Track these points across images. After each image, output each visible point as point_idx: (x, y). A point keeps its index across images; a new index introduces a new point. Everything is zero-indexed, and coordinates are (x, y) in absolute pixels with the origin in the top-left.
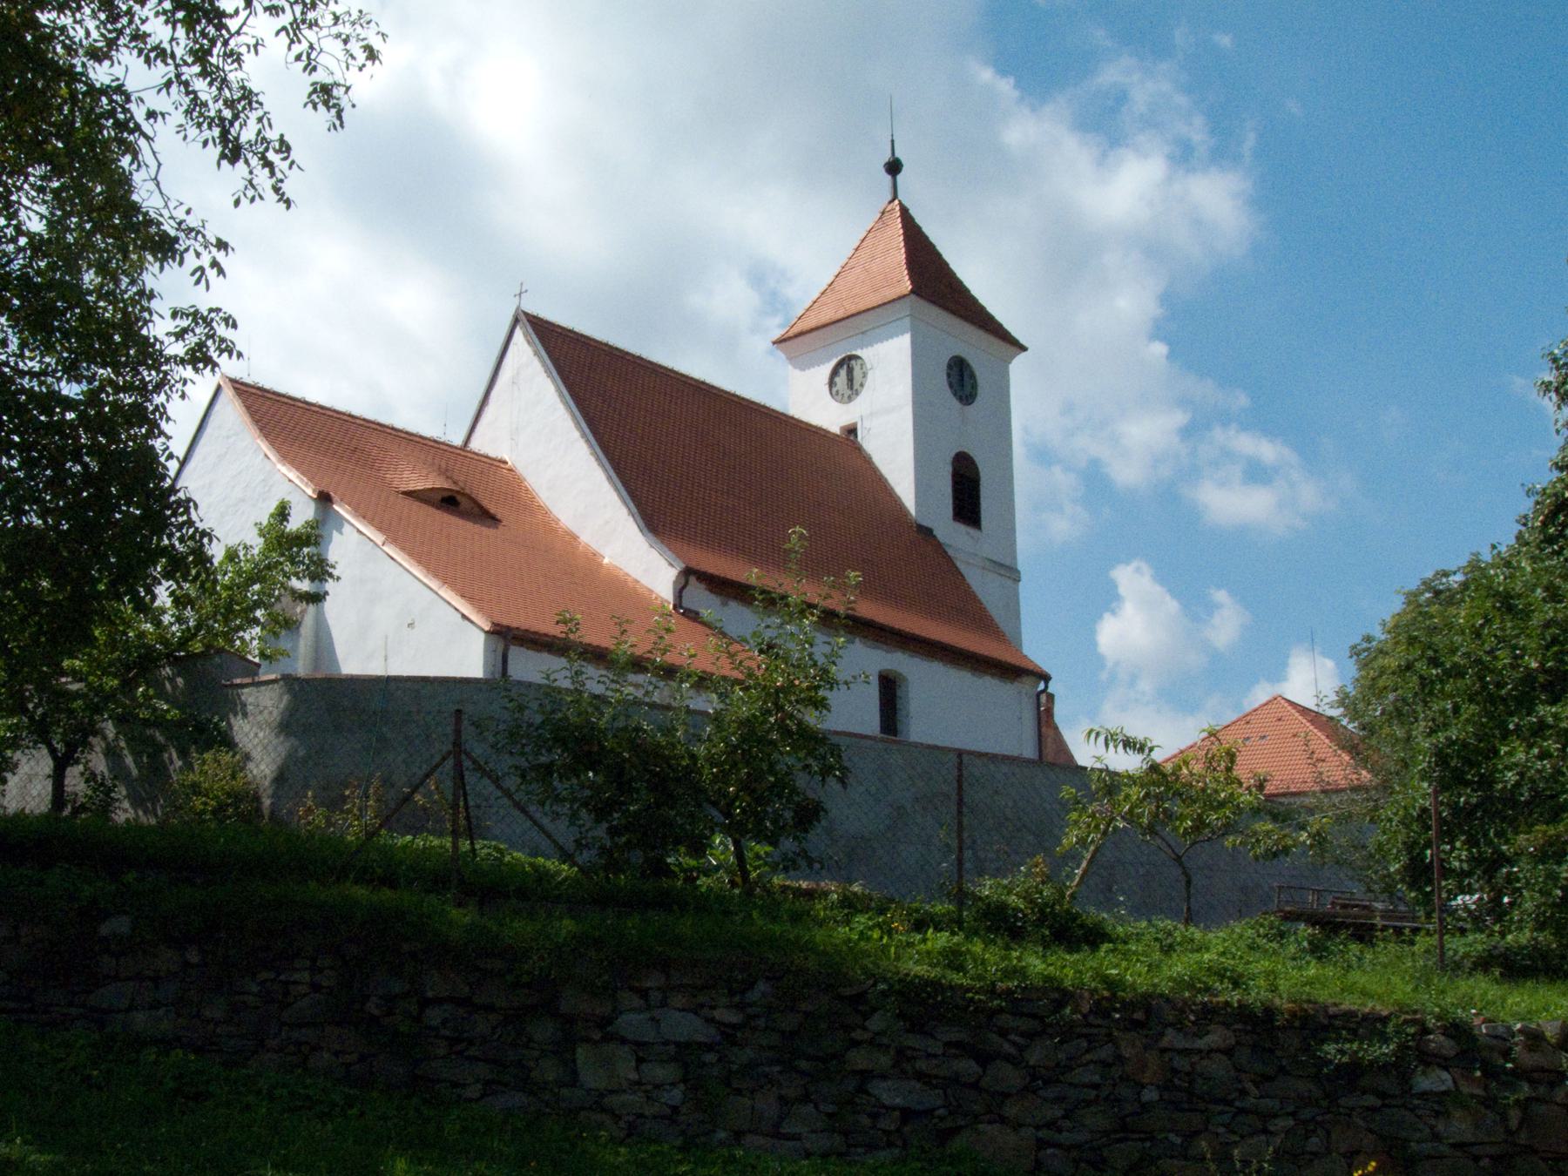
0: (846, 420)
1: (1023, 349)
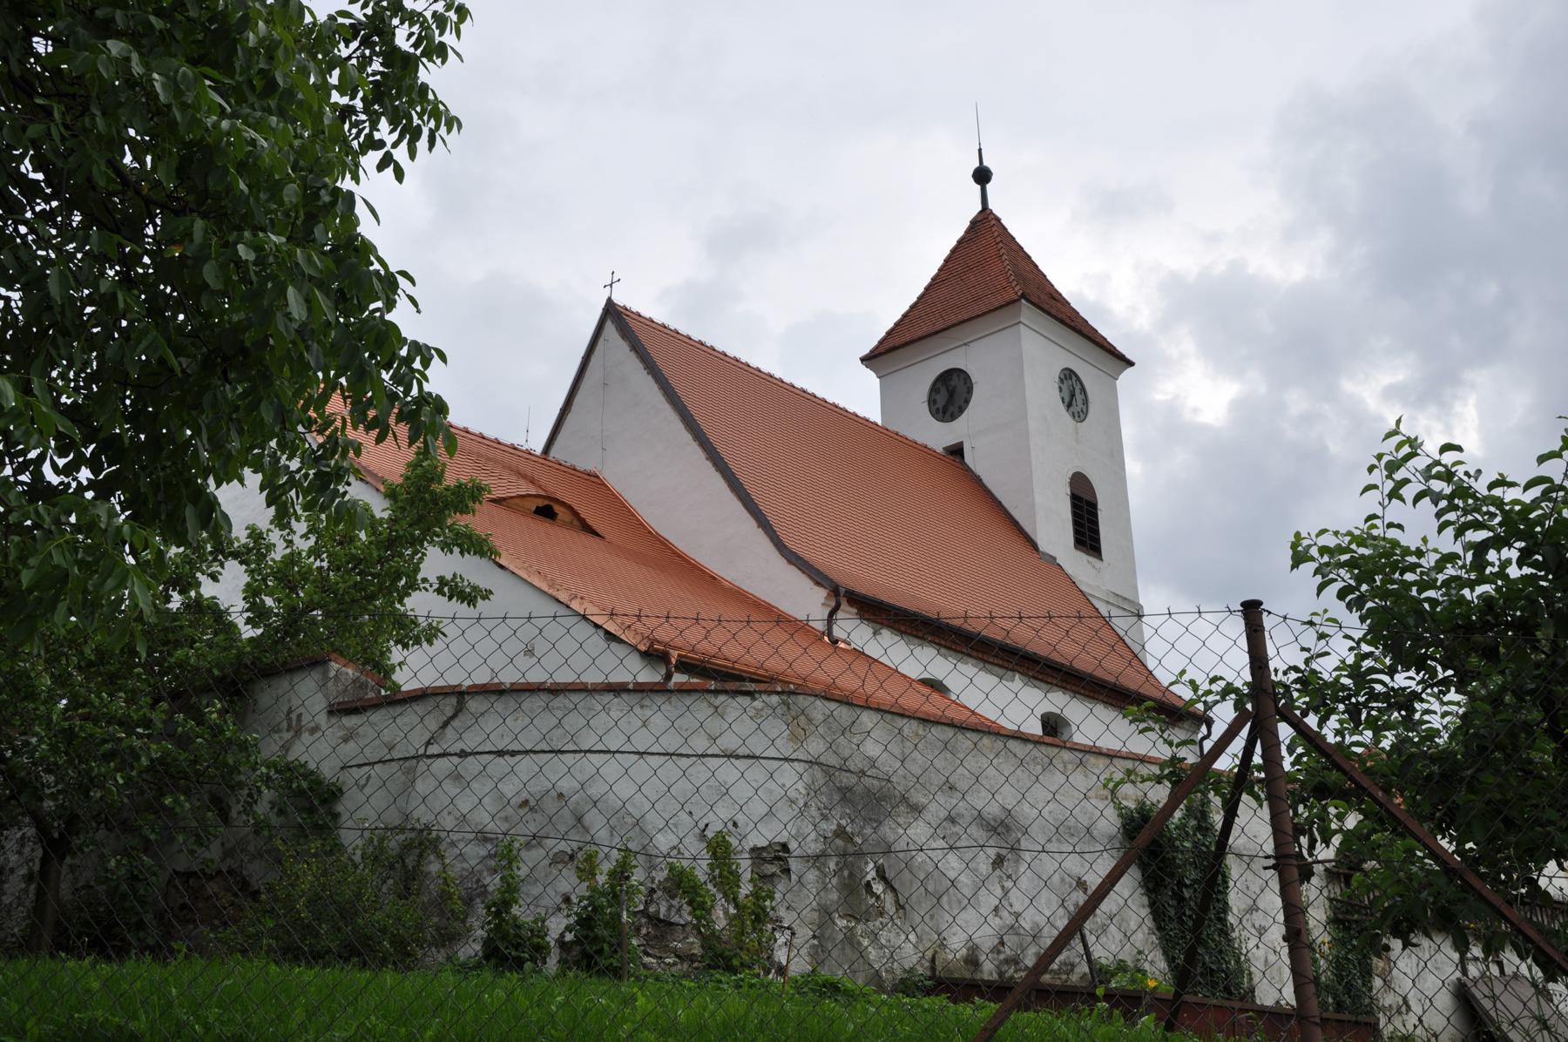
0: (951, 441)
1: (1131, 364)
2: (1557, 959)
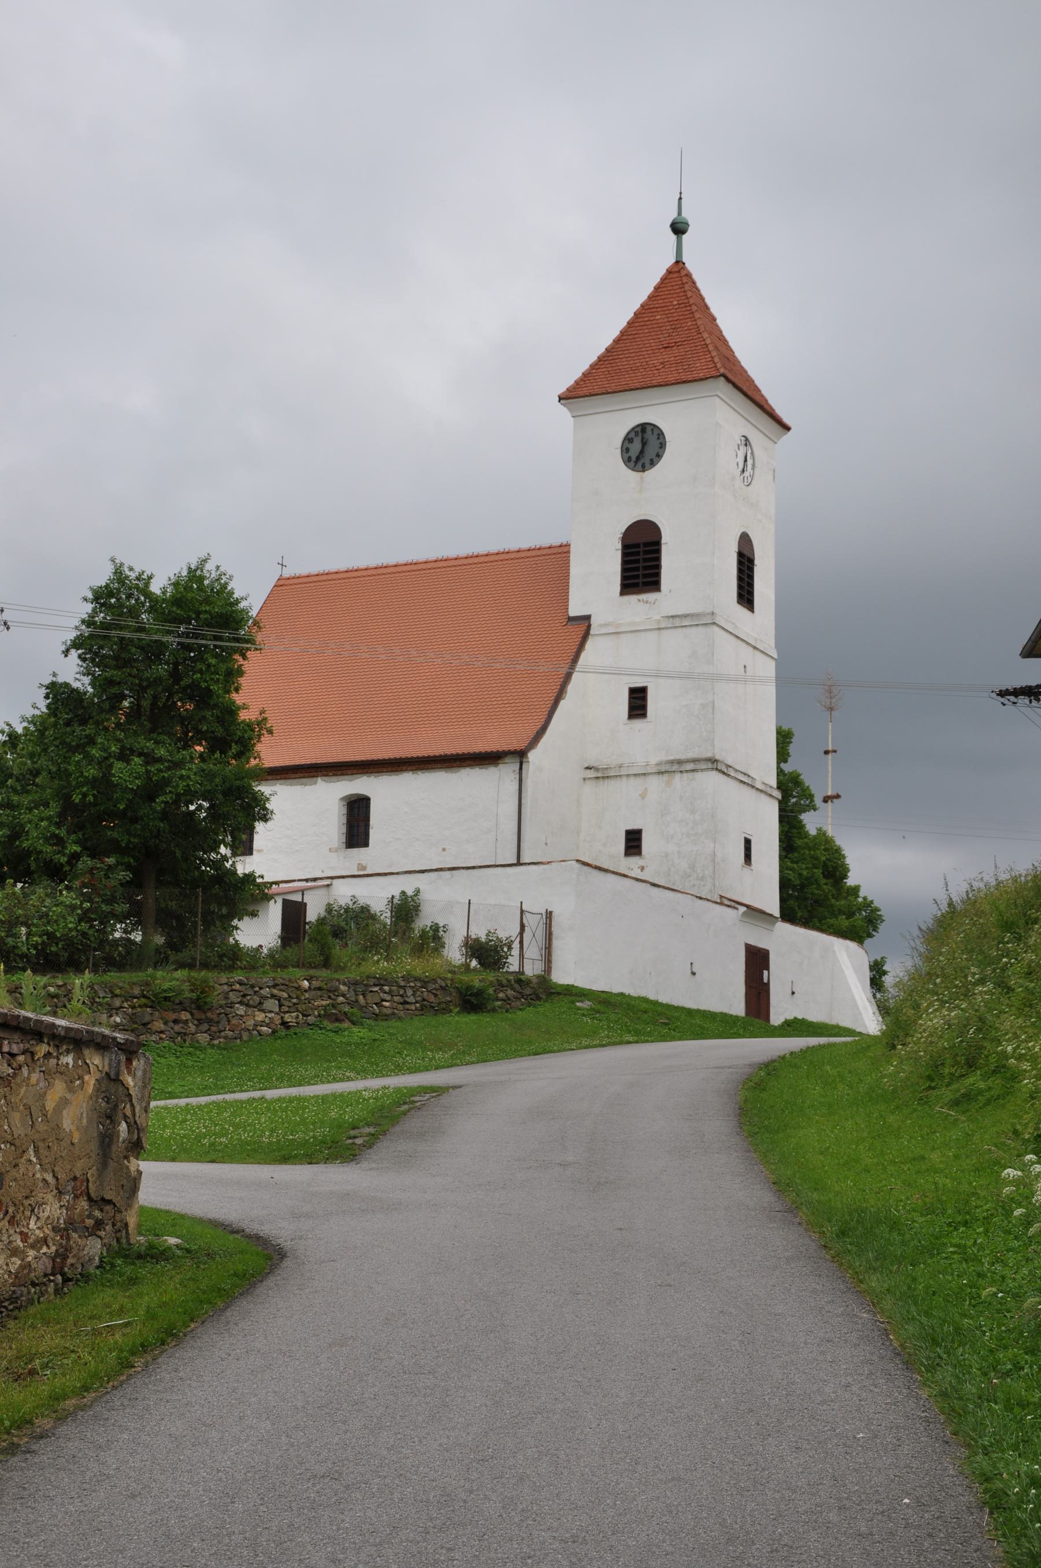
1: (788, 428)
2: (32, 1016)
